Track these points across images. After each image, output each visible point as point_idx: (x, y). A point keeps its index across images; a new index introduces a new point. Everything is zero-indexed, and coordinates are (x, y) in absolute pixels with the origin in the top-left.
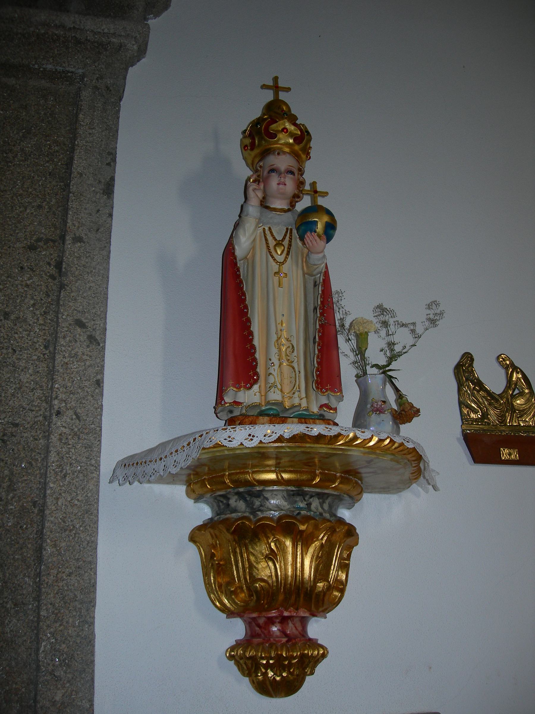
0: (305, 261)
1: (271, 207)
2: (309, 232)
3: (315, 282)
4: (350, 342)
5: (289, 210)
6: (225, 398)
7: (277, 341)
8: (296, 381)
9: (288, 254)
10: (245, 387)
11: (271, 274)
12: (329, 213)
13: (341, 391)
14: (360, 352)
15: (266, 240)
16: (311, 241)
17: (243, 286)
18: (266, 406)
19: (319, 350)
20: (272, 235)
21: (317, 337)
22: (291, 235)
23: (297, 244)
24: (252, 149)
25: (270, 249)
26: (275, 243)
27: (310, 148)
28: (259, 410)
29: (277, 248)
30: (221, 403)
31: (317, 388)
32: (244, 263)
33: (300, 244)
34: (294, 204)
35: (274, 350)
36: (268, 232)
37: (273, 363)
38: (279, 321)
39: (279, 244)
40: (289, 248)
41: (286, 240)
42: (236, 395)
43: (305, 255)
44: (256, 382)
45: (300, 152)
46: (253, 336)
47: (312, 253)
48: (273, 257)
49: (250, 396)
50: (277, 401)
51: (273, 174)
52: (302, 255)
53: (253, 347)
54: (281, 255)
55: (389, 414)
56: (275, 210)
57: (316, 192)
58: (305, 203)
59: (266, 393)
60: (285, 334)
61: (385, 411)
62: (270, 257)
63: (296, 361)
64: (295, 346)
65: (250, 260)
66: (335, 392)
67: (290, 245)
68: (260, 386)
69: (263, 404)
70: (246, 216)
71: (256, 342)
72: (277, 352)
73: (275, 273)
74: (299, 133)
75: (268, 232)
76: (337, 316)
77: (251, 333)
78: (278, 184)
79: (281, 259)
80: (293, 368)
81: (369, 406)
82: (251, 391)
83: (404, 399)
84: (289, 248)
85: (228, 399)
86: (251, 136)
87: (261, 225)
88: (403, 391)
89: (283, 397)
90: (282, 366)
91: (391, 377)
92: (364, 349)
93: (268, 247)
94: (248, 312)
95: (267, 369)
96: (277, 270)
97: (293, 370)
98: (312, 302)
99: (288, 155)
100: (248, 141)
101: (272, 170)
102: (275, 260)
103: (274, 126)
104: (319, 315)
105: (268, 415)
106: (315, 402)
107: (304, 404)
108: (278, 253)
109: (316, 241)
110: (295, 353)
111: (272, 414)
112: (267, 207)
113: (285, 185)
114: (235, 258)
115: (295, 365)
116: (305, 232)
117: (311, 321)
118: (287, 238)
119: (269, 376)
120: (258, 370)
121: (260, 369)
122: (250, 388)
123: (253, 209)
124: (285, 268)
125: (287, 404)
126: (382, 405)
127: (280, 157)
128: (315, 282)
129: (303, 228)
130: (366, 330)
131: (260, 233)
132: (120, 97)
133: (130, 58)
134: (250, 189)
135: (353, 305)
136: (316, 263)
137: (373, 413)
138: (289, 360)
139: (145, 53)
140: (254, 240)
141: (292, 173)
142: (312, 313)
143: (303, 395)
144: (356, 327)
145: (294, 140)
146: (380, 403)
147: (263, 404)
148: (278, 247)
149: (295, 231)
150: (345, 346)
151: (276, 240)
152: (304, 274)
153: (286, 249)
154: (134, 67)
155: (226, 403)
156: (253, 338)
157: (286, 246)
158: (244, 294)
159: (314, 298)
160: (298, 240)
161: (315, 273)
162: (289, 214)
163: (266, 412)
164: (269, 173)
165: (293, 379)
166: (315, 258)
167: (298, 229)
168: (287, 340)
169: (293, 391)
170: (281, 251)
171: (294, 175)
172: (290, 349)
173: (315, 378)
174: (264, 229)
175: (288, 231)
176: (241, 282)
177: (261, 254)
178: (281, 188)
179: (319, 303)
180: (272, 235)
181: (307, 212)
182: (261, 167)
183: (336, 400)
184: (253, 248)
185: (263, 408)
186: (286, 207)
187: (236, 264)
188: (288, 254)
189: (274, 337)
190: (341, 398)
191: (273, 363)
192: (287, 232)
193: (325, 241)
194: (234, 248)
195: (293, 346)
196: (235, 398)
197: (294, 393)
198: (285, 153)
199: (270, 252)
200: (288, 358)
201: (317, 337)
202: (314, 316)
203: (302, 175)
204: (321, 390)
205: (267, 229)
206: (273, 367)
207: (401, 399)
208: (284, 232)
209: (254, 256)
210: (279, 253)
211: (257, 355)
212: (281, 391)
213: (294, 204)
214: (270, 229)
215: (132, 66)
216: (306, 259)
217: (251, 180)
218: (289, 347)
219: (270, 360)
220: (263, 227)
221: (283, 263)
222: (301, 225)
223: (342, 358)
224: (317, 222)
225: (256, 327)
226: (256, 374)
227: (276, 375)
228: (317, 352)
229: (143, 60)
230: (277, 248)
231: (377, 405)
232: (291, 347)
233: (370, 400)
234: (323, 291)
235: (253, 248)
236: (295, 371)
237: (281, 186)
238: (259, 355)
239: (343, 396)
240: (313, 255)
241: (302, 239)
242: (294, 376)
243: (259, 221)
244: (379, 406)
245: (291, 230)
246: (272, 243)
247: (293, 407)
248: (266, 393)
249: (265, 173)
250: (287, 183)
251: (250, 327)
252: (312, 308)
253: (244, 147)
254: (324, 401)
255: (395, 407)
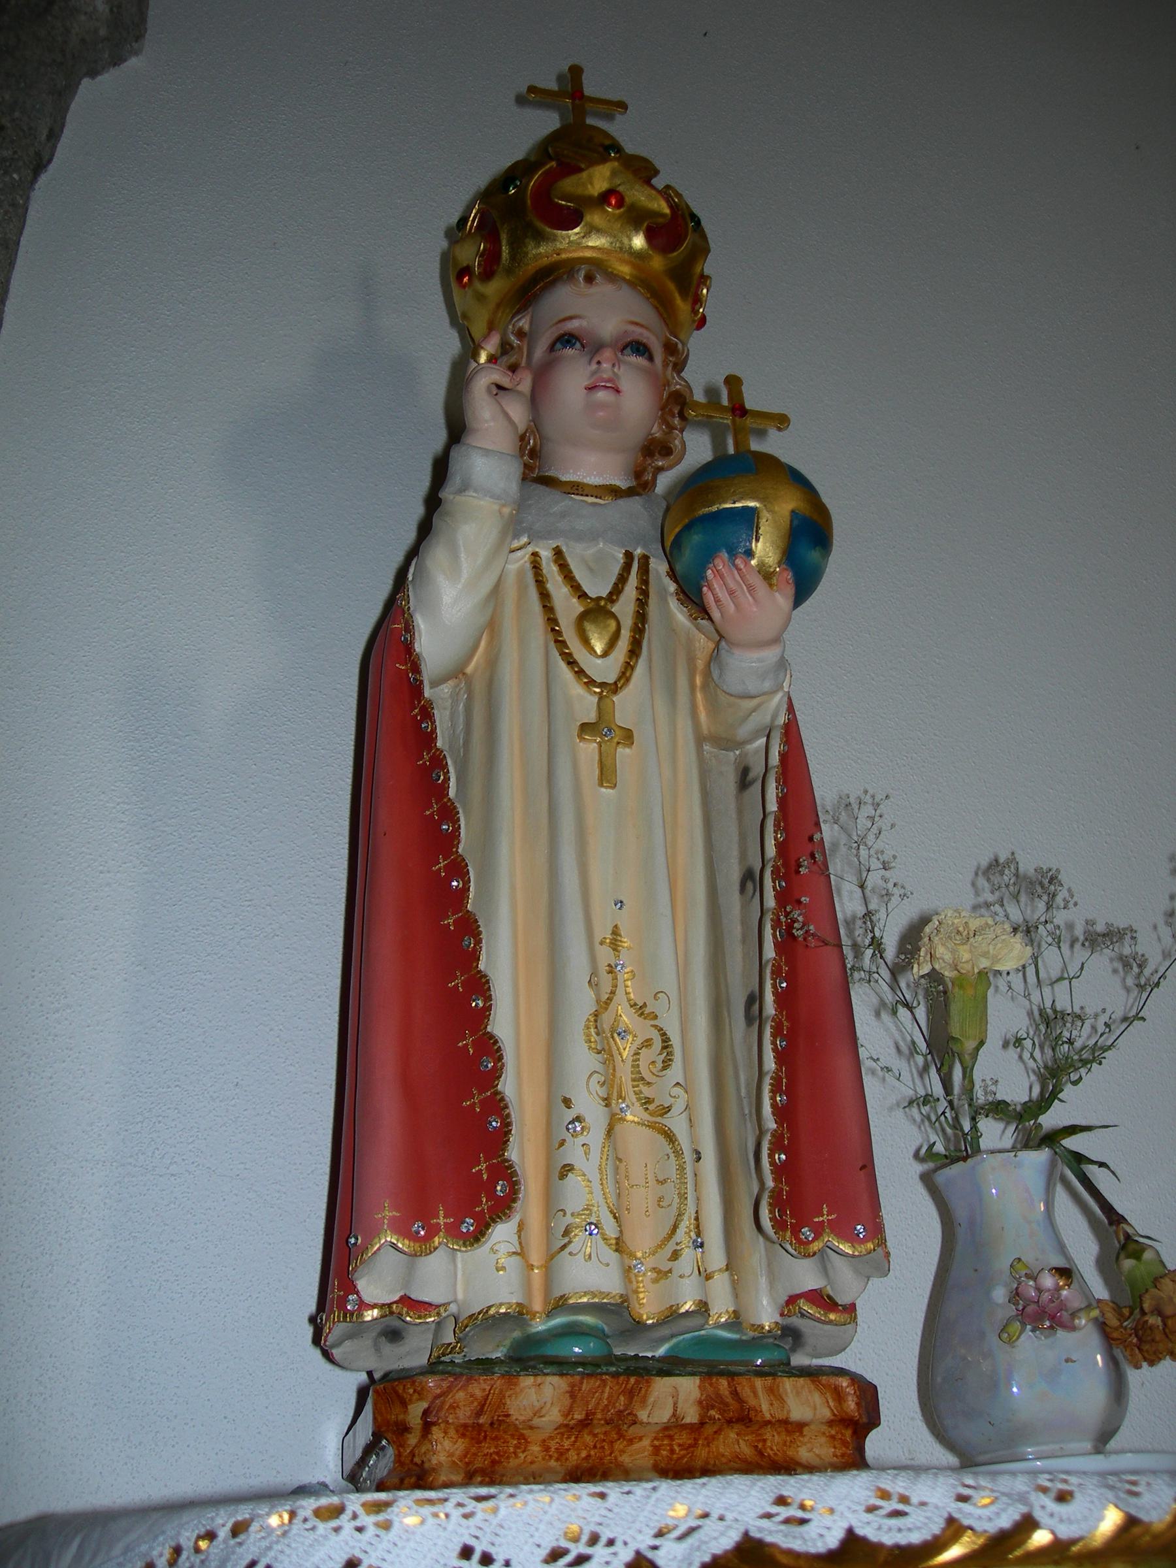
0: (705, 686)
1: (564, 479)
2: (725, 555)
3: (745, 771)
4: (903, 1012)
5: (630, 492)
6: (361, 1285)
7: (596, 1015)
8: (683, 1197)
9: (635, 650)
10: (454, 1232)
11: (567, 733)
12: (798, 479)
13: (877, 1231)
14: (943, 1049)
15: (545, 596)
16: (731, 593)
17: (447, 779)
18: (549, 1315)
19: (780, 1057)
20: (568, 576)
21: (769, 998)
22: (644, 579)
23: (667, 615)
24: (488, 275)
25: (559, 633)
26: (578, 607)
27: (704, 279)
28: (517, 1334)
29: (588, 626)
30: (343, 1302)
31: (779, 1225)
32: (454, 697)
33: (680, 615)
34: (648, 477)
35: (581, 1060)
36: (551, 570)
37: (578, 1119)
38: (602, 931)
39: (596, 611)
40: (639, 630)
41: (623, 598)
42: (409, 1275)
43: (700, 664)
44: (502, 1207)
45: (671, 286)
46: (488, 998)
47: (731, 644)
48: (571, 662)
49: (479, 1275)
50: (602, 1294)
51: (569, 352)
52: (691, 660)
53: (490, 1046)
54: (605, 654)
55: (1090, 1325)
56: (577, 488)
57: (739, 410)
58: (697, 448)
59: (551, 1256)
60: (630, 988)
61: (1074, 1315)
62: (563, 665)
63: (679, 1106)
64: (675, 1041)
65: (484, 695)
66: (853, 1239)
67: (641, 617)
68: (521, 1227)
69: (537, 1305)
70: (462, 490)
71: (501, 1025)
72: (599, 1067)
73: (585, 728)
74: (667, 211)
75: (551, 570)
76: (848, 904)
77: (480, 985)
78: (591, 388)
79: (605, 669)
80: (670, 1137)
81: (1000, 1294)
82: (482, 1252)
83: (1148, 1255)
84: (639, 630)
85: (376, 1286)
86: (488, 230)
87: (524, 540)
88: (1140, 1216)
89: (627, 1271)
90: (618, 1128)
91: (1078, 1159)
92: (970, 1045)
93: (552, 621)
94: (466, 889)
95: (554, 1144)
96: (592, 717)
97: (668, 1149)
98: (735, 853)
99: (625, 287)
100: (470, 253)
101: (568, 339)
102: (580, 673)
103: (568, 184)
104: (771, 902)
105: (561, 1365)
106: (763, 1281)
107: (721, 1308)
108: (592, 650)
109: (751, 589)
110: (676, 1072)
111: (581, 1362)
112: (549, 482)
113: (618, 391)
114: (416, 668)
115: (677, 1123)
116: (706, 557)
117: (734, 929)
118: (633, 580)
119: (562, 1176)
120: (513, 1153)
121: (524, 1151)
122: (476, 1237)
123: (488, 467)
124: (627, 707)
125: (648, 1308)
126: (1058, 1289)
127: (594, 290)
128: (745, 771)
129: (696, 538)
130: (984, 963)
131: (520, 573)
132: (38, 154)
133: (83, 41)
134: (481, 384)
135: (909, 858)
136: (752, 686)
137: (1024, 1325)
138: (649, 1101)
139: (139, 37)
140: (496, 590)
141: (640, 348)
142: (736, 895)
143: (716, 1257)
144: (940, 951)
145: (650, 237)
146: (1048, 1281)
147: (537, 1305)
148: (594, 621)
149: (659, 567)
150: (882, 1036)
151: (583, 595)
152: (700, 740)
153: (626, 634)
154: (99, 78)
155: (363, 1305)
156: (488, 1009)
157: (627, 622)
158: (449, 813)
159: (743, 836)
160: (674, 604)
161: (743, 732)
162: (634, 504)
163: (552, 1350)
164: (552, 348)
165: (670, 1191)
166: (746, 666)
167: (671, 554)
168: (640, 1010)
169: (671, 1247)
170: (606, 638)
171: (651, 359)
172: (653, 1053)
173: (770, 1183)
174: (535, 554)
175: (633, 565)
176: (438, 762)
177: (524, 650)
178: (600, 417)
179: (771, 851)
180: (568, 576)
181: (702, 484)
182: (520, 334)
183: (857, 1271)
184: (492, 626)
185: (539, 1326)
186: (622, 483)
187: (416, 690)
188: (635, 650)
189: (582, 1002)
190: (878, 1263)
191: (578, 1119)
192: (627, 567)
193: (790, 591)
194: (409, 628)
195: (665, 1039)
196: (407, 1283)
197: (675, 1255)
198: (612, 277)
199: (561, 644)
200: (647, 1091)
201: (769, 998)
202: (745, 906)
203: (679, 367)
204: (796, 1232)
205: (546, 554)
206: (581, 1140)
207: (1137, 1254)
208: (616, 569)
209: (493, 662)
210: (599, 648)
211: (507, 1086)
212: (619, 1246)
213: (648, 477)
214: (558, 553)
215: (93, 73)
216: (707, 673)
217: (483, 358)
218: (647, 1043)
219: (567, 1102)
220: (530, 549)
221: (615, 688)
222: (688, 527)
223: (871, 1086)
224: (753, 510)
225: (502, 959)
226: (505, 1172)
227: (595, 1176)
228: (770, 1064)
229: (133, 61)
230: (588, 626)
231: (1039, 1290)
232: (658, 1044)
233: (1003, 1263)
234: (782, 802)
235: (492, 626)
236: (678, 1153)
237: (601, 395)
238: (519, 1086)
239: (888, 1254)
240: (737, 652)
241: (692, 596)
242: (673, 1174)
243: (514, 526)
244: (1046, 1296)
245: (645, 560)
246: (568, 607)
247: (672, 1316)
248: (551, 1256)
249: (540, 351)
250: (625, 385)
251: (474, 956)
252: (736, 876)
253: (455, 274)
254: (806, 1276)
255: (1100, 1291)
